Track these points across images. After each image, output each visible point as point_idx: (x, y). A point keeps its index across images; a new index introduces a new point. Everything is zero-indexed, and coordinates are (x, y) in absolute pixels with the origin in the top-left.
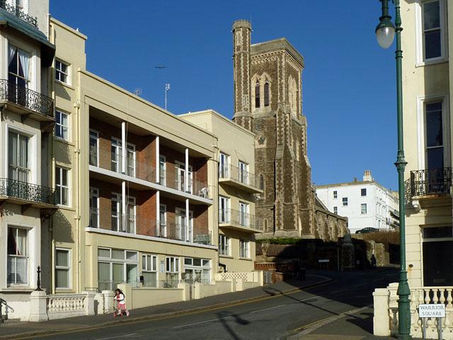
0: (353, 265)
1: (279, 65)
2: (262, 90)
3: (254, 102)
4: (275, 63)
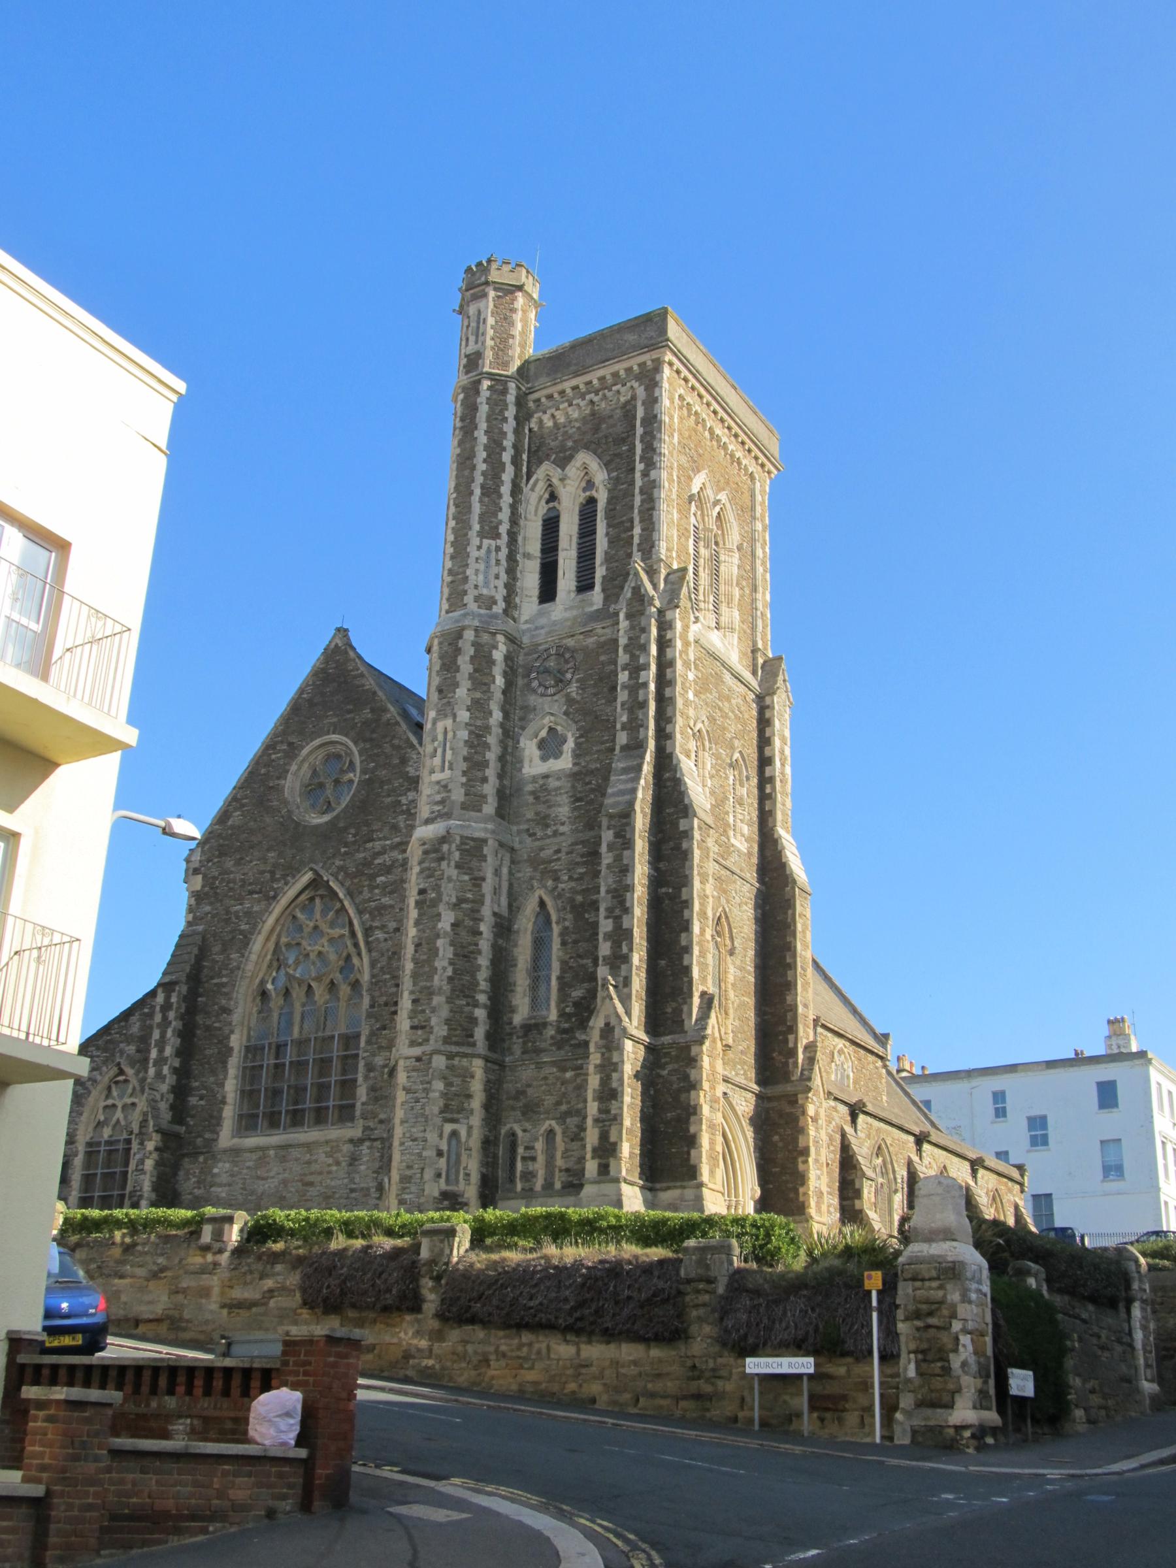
0: (981, 1403)
1: (640, 413)
2: (569, 528)
3: (530, 580)
4: (628, 411)
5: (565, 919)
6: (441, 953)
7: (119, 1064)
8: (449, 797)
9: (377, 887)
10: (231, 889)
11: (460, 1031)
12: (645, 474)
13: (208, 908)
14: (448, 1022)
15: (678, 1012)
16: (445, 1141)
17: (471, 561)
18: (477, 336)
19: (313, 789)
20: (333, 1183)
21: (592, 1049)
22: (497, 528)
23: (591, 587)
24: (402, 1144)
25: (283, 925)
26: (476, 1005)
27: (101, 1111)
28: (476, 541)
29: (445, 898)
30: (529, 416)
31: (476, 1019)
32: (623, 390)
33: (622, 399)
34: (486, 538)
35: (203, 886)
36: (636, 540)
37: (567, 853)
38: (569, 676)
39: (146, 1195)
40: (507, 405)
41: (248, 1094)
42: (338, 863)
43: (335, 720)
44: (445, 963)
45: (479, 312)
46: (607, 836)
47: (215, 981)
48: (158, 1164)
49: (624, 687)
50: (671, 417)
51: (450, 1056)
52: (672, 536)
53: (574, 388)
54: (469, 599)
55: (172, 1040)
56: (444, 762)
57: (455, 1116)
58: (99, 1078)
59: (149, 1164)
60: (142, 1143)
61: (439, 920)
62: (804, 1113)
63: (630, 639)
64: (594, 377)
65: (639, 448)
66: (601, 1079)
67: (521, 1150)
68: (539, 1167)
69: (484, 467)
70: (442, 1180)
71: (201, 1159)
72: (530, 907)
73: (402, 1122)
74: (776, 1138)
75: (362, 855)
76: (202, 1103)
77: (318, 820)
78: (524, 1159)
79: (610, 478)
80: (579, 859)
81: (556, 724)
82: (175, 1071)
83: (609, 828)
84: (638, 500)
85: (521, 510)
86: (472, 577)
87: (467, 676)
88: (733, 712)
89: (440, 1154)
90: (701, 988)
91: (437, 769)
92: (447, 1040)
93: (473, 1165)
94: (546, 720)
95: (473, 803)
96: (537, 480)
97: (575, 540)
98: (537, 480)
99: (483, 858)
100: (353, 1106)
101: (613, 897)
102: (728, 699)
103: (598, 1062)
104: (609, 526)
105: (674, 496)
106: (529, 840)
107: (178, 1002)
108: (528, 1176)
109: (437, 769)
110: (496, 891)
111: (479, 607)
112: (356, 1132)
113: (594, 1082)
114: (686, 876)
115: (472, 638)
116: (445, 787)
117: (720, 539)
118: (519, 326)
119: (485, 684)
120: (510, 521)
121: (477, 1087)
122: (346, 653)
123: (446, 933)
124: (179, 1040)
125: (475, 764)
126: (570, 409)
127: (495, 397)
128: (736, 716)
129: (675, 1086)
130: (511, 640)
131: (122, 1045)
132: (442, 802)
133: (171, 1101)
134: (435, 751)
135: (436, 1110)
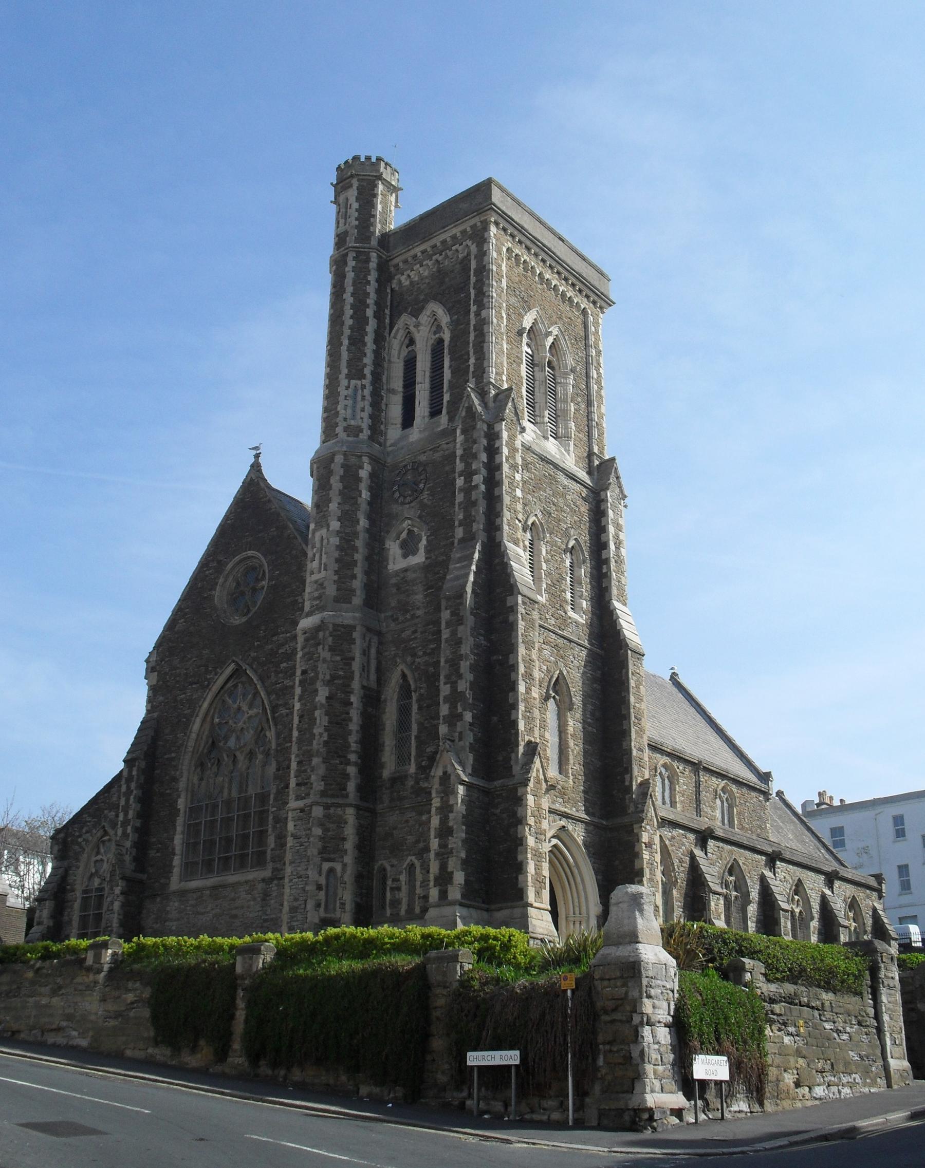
1: (473, 265)
3: (395, 410)
4: (465, 264)
5: (420, 688)
6: (318, 721)
7: (104, 827)
8: (324, 593)
9: (281, 672)
10: (178, 682)
11: (335, 785)
12: (478, 314)
13: (161, 698)
14: (324, 779)
15: (508, 760)
16: (323, 876)
17: (341, 398)
18: (346, 219)
19: (235, 598)
20: (251, 915)
21: (434, 795)
22: (362, 370)
23: (440, 412)
24: (291, 881)
25: (215, 708)
26: (348, 763)
27: (92, 864)
28: (344, 382)
29: (321, 676)
30: (390, 278)
31: (348, 775)
32: (460, 248)
33: (461, 256)
34: (353, 379)
35: (158, 681)
36: (472, 369)
37: (422, 633)
38: (421, 486)
39: (115, 930)
40: (369, 271)
41: (191, 846)
42: (253, 654)
43: (250, 539)
44: (321, 730)
45: (347, 199)
46: (446, 615)
47: (166, 757)
48: (123, 905)
49: (461, 490)
50: (499, 266)
51: (327, 807)
52: (502, 363)
53: (423, 252)
54: (339, 430)
55: (134, 805)
56: (320, 564)
57: (332, 856)
58: (90, 838)
59: (117, 905)
60: (112, 889)
61: (317, 695)
62: (638, 840)
63: (464, 450)
64: (437, 241)
66: (441, 818)
67: (389, 882)
68: (403, 895)
69: (351, 322)
70: (322, 909)
71: (158, 900)
72: (394, 680)
73: (291, 863)
74: (617, 862)
75: (270, 647)
76: (159, 854)
77: (238, 620)
78: (392, 889)
79: (452, 322)
80: (430, 637)
81: (413, 526)
82: (136, 830)
83: (446, 609)
85: (385, 354)
86: (342, 412)
87: (337, 493)
88: (567, 506)
89: (319, 888)
90: (527, 738)
91: (316, 571)
92: (323, 794)
93: (347, 896)
94: (405, 525)
95: (344, 596)
96: (399, 329)
97: (428, 374)
98: (399, 329)
99: (353, 642)
100: (265, 852)
101: (450, 666)
102: (563, 496)
103: (438, 805)
104: (451, 360)
105: (503, 330)
106: (393, 625)
107: (138, 775)
108: (396, 903)
109: (316, 571)
110: (365, 669)
111: (348, 436)
112: (267, 873)
113: (435, 822)
114: (513, 644)
115: (342, 461)
116: (320, 585)
117: (555, 363)
118: (379, 207)
119: (353, 498)
120: (374, 364)
121: (350, 831)
122: (258, 484)
123: (322, 705)
124: (139, 805)
125: (344, 565)
126: (421, 269)
127: (360, 265)
128: (571, 509)
129: (506, 822)
130: (374, 460)
131: (106, 812)
132: (319, 598)
133: (134, 854)
134: (314, 556)
135: (315, 852)
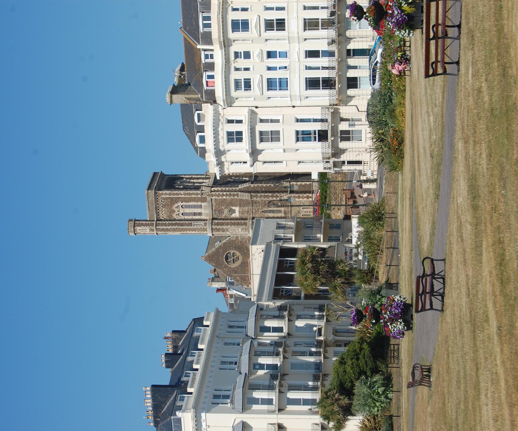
65: (175, 196)
84: (187, 196)
95: (245, 224)
